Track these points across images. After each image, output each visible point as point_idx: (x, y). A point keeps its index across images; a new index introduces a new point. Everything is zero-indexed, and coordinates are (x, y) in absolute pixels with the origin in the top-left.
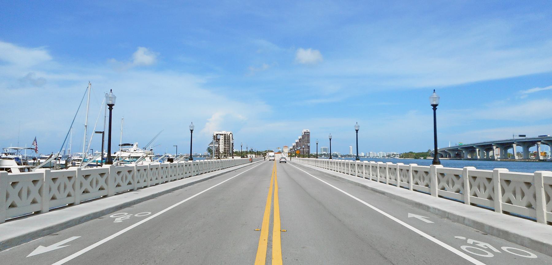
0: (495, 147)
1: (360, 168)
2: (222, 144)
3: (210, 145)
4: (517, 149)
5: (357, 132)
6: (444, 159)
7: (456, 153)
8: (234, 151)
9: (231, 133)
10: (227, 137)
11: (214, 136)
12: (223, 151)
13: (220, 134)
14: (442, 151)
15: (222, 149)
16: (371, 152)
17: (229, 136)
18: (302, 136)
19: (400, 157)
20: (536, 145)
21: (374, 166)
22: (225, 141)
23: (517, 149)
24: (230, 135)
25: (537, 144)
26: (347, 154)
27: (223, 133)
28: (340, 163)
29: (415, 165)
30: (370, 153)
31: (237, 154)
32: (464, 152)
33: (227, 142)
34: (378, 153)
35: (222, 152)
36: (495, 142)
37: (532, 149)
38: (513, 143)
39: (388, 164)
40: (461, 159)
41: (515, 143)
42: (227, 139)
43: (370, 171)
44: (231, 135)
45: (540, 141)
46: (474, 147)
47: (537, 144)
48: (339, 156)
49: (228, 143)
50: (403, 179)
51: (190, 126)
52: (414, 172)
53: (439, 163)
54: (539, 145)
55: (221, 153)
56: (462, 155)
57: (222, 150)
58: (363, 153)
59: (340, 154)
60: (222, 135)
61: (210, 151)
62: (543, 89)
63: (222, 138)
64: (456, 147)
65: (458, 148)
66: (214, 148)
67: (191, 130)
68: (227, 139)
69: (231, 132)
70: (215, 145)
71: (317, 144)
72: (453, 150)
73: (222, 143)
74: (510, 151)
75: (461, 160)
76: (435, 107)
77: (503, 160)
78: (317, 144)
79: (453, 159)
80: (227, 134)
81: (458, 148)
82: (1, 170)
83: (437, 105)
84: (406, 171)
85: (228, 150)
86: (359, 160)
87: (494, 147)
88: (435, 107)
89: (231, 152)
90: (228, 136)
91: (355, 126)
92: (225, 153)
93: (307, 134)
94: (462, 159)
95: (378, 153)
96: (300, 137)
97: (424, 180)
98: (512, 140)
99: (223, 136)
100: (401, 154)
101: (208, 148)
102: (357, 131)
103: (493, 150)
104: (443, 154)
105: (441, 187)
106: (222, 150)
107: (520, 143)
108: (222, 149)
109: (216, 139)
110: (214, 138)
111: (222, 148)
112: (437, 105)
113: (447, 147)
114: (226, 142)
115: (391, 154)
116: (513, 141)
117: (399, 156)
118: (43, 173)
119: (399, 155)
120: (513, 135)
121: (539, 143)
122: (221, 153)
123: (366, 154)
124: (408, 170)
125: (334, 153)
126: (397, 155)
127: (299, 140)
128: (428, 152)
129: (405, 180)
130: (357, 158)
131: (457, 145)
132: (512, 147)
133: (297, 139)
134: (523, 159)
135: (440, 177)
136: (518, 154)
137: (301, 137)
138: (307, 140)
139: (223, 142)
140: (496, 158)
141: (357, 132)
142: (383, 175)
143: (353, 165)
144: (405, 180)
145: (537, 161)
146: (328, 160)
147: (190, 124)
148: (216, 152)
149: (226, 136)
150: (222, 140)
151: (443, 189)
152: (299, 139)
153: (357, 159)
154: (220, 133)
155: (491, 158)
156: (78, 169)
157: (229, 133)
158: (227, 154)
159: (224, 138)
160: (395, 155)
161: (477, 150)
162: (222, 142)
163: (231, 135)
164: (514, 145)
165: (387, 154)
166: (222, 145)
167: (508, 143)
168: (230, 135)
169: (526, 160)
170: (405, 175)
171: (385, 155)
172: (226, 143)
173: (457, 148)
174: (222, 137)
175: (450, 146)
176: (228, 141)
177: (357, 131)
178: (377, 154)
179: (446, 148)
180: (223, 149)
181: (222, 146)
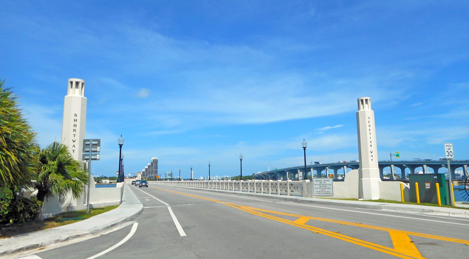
1: (211, 184)
14: (262, 175)
18: (151, 163)
19: (231, 180)
21: (222, 183)
24: (86, 162)
25: (326, 169)
26: (189, 178)
34: (214, 177)
36: (286, 169)
43: (216, 185)
45: (328, 167)
46: (275, 173)
50: (251, 188)
59: (183, 178)
65: (274, 172)
74: (323, 172)
76: (121, 146)
82: (5, 235)
83: (122, 145)
84: (267, 184)
87: (299, 171)
88: (121, 146)
95: (214, 177)
96: (149, 164)
97: (275, 187)
98: (310, 166)
100: (233, 177)
104: (263, 177)
105: (291, 191)
107: (315, 168)
112: (122, 145)
113: (267, 171)
115: (225, 178)
116: (311, 167)
117: (230, 179)
118: (455, 201)
119: (231, 178)
120: (391, 154)
121: (327, 168)
123: (205, 178)
124: (268, 184)
125: (178, 178)
126: (229, 178)
127: (148, 167)
128: (253, 176)
129: (252, 188)
130: (191, 180)
131: (274, 170)
133: (146, 166)
135: (291, 186)
137: (148, 167)
140: (300, 179)
142: (227, 187)
143: (189, 183)
144: (252, 188)
147: (303, 142)
151: (292, 191)
152: (148, 166)
153: (241, 179)
155: (296, 179)
156: (370, 178)
160: (228, 178)
161: (287, 173)
164: (312, 170)
165: (222, 178)
167: (323, 167)
168: (86, 162)
170: (266, 186)
171: (220, 179)
175: (269, 171)
178: (213, 178)
179: (265, 173)
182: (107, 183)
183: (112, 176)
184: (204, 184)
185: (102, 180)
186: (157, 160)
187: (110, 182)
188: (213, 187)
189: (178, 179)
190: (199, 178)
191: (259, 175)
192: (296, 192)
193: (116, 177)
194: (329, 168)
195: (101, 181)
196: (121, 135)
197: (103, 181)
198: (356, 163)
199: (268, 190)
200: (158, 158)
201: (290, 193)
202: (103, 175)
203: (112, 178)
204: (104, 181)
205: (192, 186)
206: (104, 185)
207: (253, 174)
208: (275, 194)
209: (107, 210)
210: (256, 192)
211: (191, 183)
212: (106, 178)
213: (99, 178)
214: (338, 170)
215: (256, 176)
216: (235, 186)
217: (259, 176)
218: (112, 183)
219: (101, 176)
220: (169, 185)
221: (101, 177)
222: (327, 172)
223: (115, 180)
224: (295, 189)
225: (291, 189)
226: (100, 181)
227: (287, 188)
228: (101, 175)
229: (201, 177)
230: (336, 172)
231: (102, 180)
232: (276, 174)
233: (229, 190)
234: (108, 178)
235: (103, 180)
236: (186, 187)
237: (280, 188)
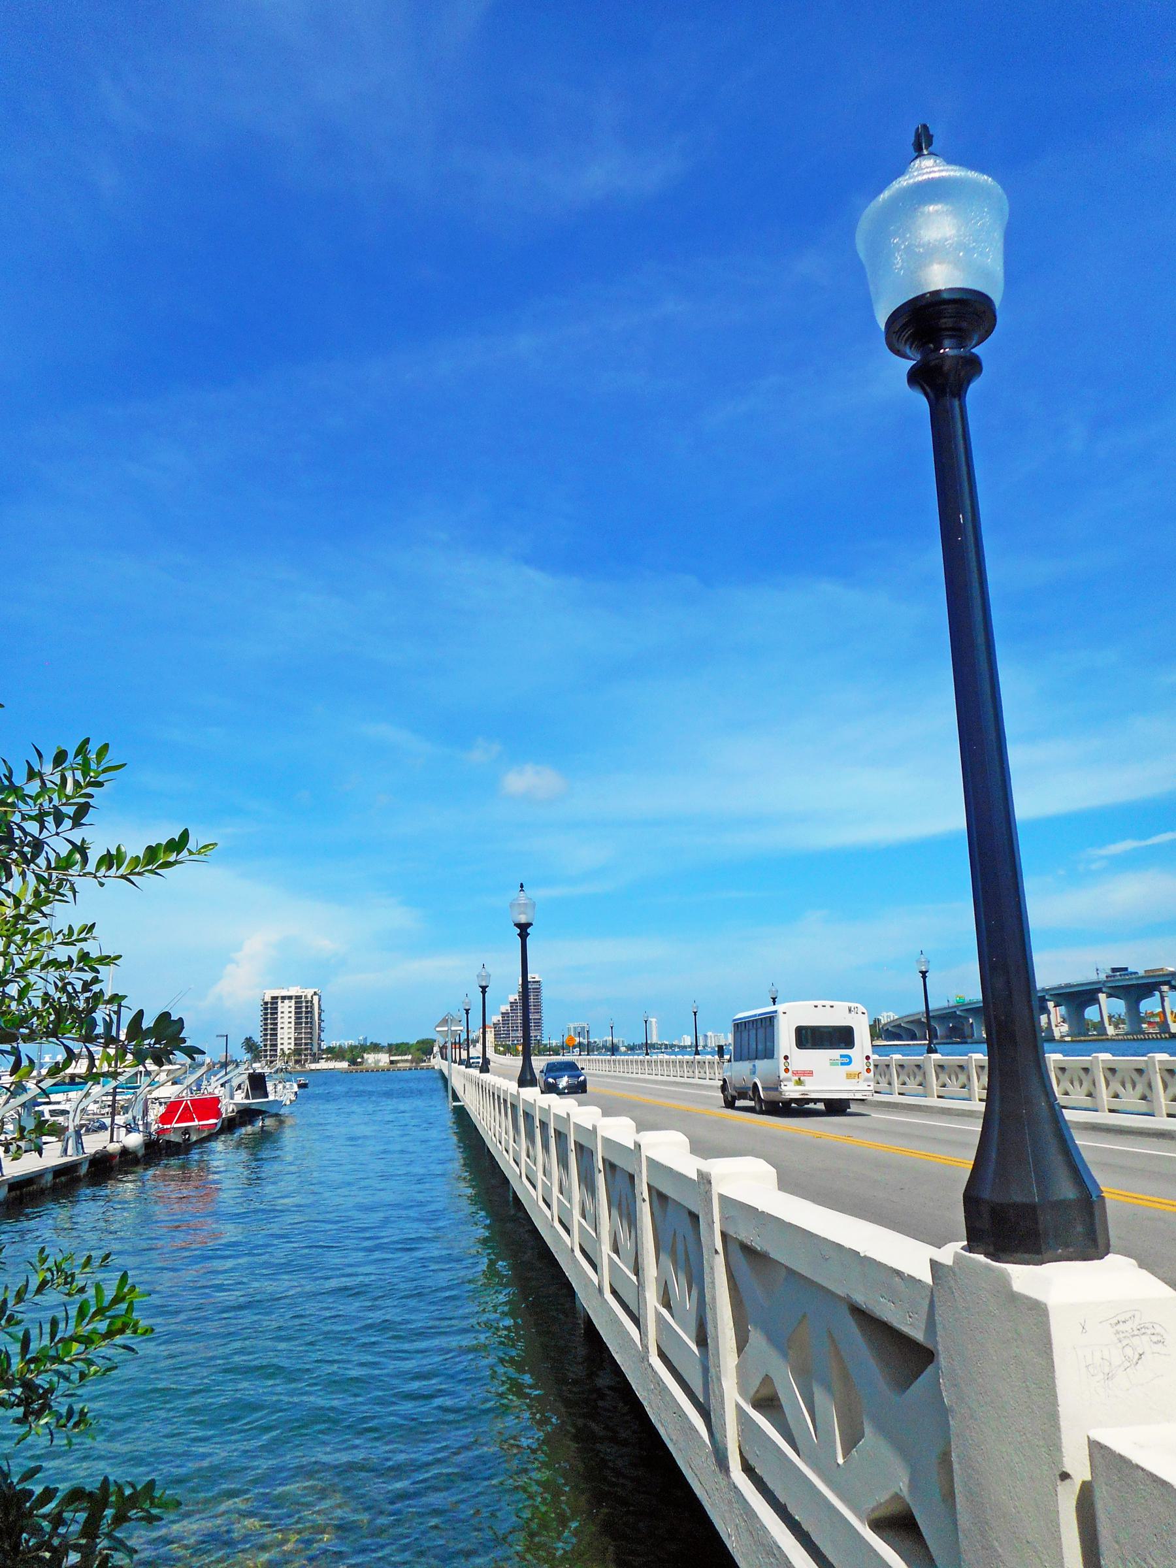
0: (1052, 1003)
2: (290, 1025)
3: (438, 1029)
4: (1110, 1006)
5: (924, 977)
6: (920, 1044)
7: (951, 1025)
8: (324, 1046)
9: (315, 993)
10: (304, 1004)
11: (266, 1003)
12: (292, 1047)
13: (284, 998)
14: (912, 1022)
15: (290, 1041)
16: (709, 1034)
17: (312, 1001)
20: (1157, 993)
22: (297, 1018)
23: (1110, 1006)
24: (312, 997)
25: (1161, 992)
27: (293, 992)
28: (709, 1063)
29: (1164, 1057)
30: (706, 1036)
31: (336, 1053)
32: (971, 1021)
33: (304, 1020)
35: (289, 1049)
37: (1149, 1005)
38: (1100, 990)
39: (1100, 1059)
40: (965, 1040)
41: (1104, 990)
42: (304, 1011)
44: (316, 998)
45: (1165, 983)
47: (1161, 992)
48: (623, 1049)
49: (306, 1023)
51: (478, 976)
52: (1165, 1073)
53: (935, 1051)
54: (1164, 994)
55: (287, 1052)
56: (967, 1031)
57: (290, 1044)
58: (689, 1037)
60: (290, 998)
61: (254, 1048)
62: (1149, 842)
63: (286, 1010)
64: (949, 1008)
65: (955, 1012)
66: (450, 1036)
67: (480, 987)
68: (304, 1010)
69: (316, 990)
70: (453, 1028)
71: (695, 1013)
72: (944, 1018)
73: (290, 1023)
74: (1091, 1013)
75: (966, 1043)
77: (1078, 1039)
78: (695, 1013)
79: (945, 1041)
80: (303, 994)
81: (955, 1012)
85: (306, 1044)
86: (699, 1054)
87: (1051, 1005)
89: (315, 1050)
90: (307, 1002)
91: (918, 961)
92: (297, 1052)
93: (533, 989)
94: (969, 1040)
97: (1134, 1087)
99: (293, 1001)
101: (247, 1039)
102: (924, 974)
103: (1049, 1014)
105: (940, 1085)
106: (290, 1044)
108: (290, 1041)
109: (270, 1009)
110: (266, 1009)
111: (290, 1038)
114: (301, 1018)
120: (1097, 970)
122: (287, 1052)
127: (511, 1006)
131: (951, 1004)
132: (1097, 1001)
134: (1126, 1034)
135: (939, 1070)
136: (1116, 1022)
138: (534, 1006)
139: (293, 1020)
141: (924, 977)
142: (712, 1071)
145: (1166, 1038)
146: (609, 1057)
147: (479, 971)
148: (271, 1050)
149: (301, 1002)
150: (290, 1015)
151: (904, 1084)
152: (511, 1003)
154: (285, 993)
157: (309, 992)
158: (306, 1055)
159: (296, 1008)
162: (290, 1020)
163: (316, 998)
166: (289, 1030)
169: (1135, 1037)
172: (301, 1023)
173: (953, 1010)
174: (290, 1004)
176: (307, 1018)
177: (924, 974)
180: (292, 1041)
181: (289, 1033)
182: (381, 1064)
183: (395, 1040)
184: (683, 1067)
185: (366, 1056)
186: (537, 982)
187: (392, 1062)
188: (708, 1073)
189: (609, 1044)
190: (680, 1038)
191: (898, 1023)
192: (954, 1087)
193: (407, 1044)
194: (1110, 996)
195: (363, 1058)
196: (522, 886)
197: (367, 1060)
198: (1164, 975)
199: (890, 1084)
200: (539, 978)
201: (979, 1092)
202: (365, 1039)
203: (398, 1046)
204: (370, 1058)
205: (650, 1072)
206: (372, 1071)
207: (875, 1021)
208: (1086, 1109)
209: (520, 1214)
210: (899, 1094)
211: (646, 1063)
212: (376, 1048)
213: (356, 1047)
214: (1143, 1001)
215: (885, 1028)
216: (1116, 1086)
217: (899, 1026)
218: (399, 1065)
219: (362, 1043)
220: (637, 1073)
221: (362, 1045)
222: (1166, 1004)
223: (405, 1055)
224: (1124, 1086)
225: (1061, 1084)
226: (359, 1060)
227: (1094, 1084)
228: (361, 1038)
229: (685, 1036)
230: (1133, 1008)
231: (366, 1056)
232: (960, 1016)
233: (939, 1097)
234: (383, 1047)
235: (369, 1053)
236: (637, 1076)
237: (1058, 1085)
